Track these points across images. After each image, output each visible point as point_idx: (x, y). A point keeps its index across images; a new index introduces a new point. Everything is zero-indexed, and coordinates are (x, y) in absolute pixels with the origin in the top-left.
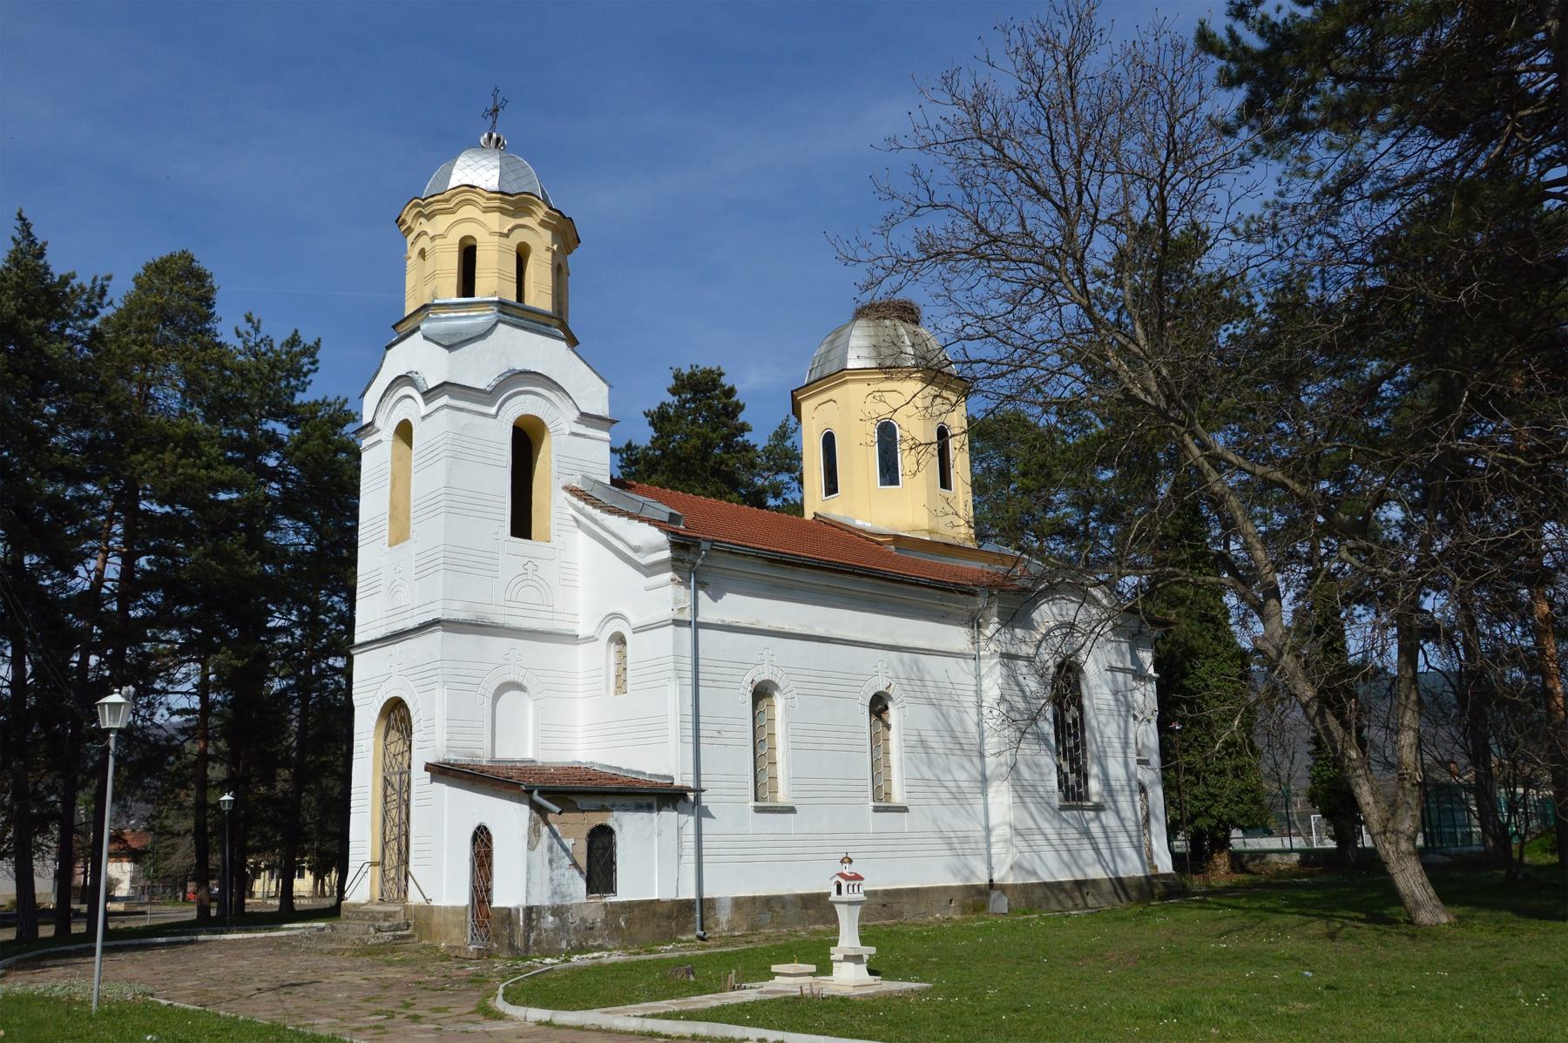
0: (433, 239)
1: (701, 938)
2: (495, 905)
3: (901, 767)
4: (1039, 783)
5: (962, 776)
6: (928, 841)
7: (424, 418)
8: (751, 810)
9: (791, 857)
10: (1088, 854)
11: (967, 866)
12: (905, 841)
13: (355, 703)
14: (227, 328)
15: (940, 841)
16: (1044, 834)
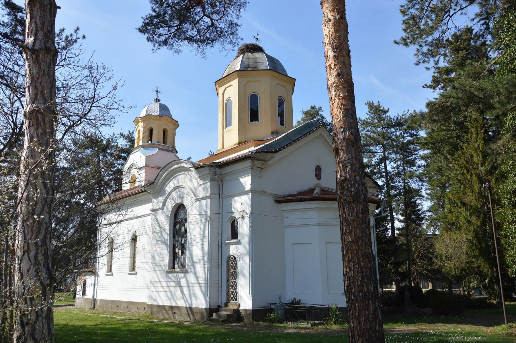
15: (145, 285)
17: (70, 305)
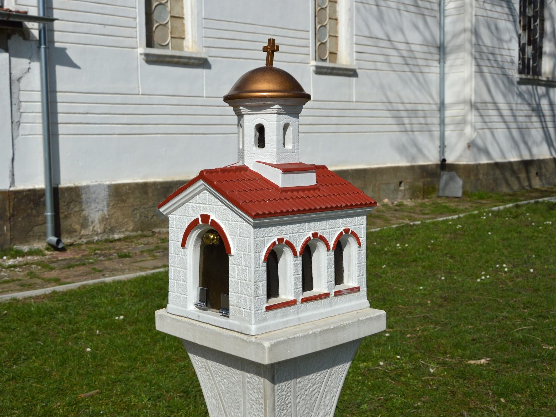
1: (54, 247)
3: (351, 19)
4: (497, 51)
5: (414, 37)
6: (376, 113)
8: (141, 60)
9: (202, 129)
10: (537, 134)
11: (415, 144)
12: (352, 113)
15: (387, 114)
16: (498, 109)
17: (144, 261)
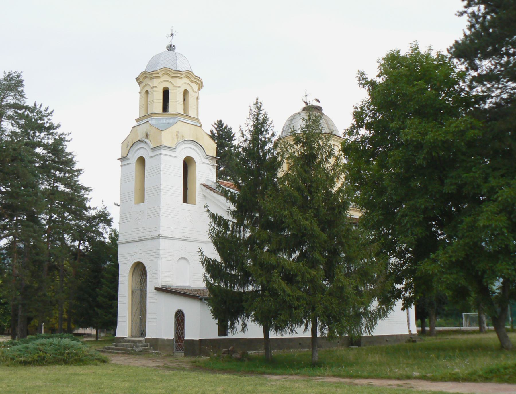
0: (152, 87)
2: (185, 339)
7: (151, 157)
13: (119, 263)
14: (403, 307)
